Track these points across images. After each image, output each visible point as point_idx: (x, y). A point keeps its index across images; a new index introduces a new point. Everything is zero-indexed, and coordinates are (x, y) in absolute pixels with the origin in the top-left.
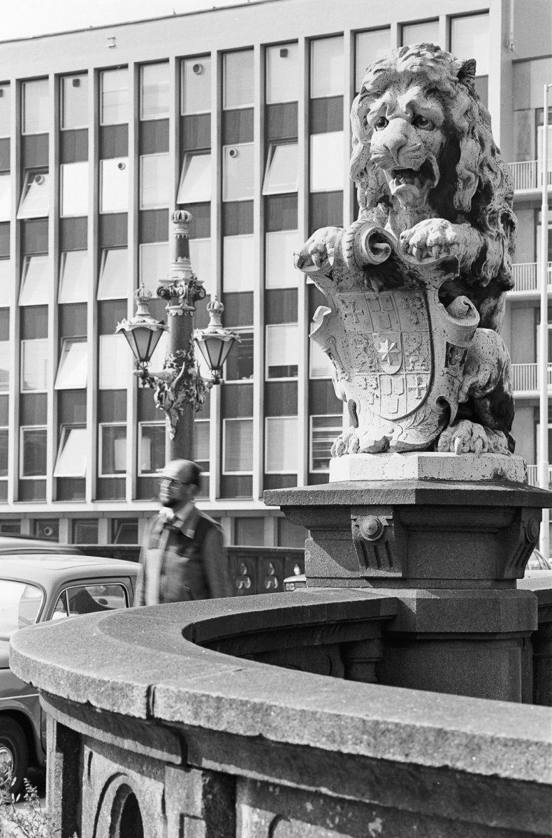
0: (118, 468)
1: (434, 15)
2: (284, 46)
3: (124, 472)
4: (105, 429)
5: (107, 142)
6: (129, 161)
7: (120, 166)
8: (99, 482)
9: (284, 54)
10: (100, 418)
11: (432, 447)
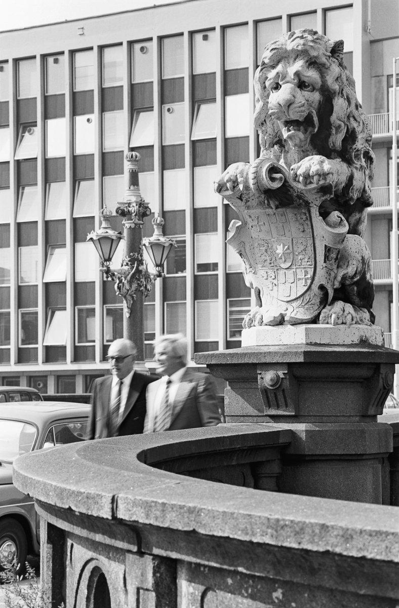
0: (89, 339)
1: (313, 9)
2: (205, 32)
3: (94, 341)
4: (79, 310)
5: (79, 104)
6: (95, 117)
7: (88, 120)
8: (76, 349)
9: (205, 38)
10: (76, 302)
11: (315, 320)
